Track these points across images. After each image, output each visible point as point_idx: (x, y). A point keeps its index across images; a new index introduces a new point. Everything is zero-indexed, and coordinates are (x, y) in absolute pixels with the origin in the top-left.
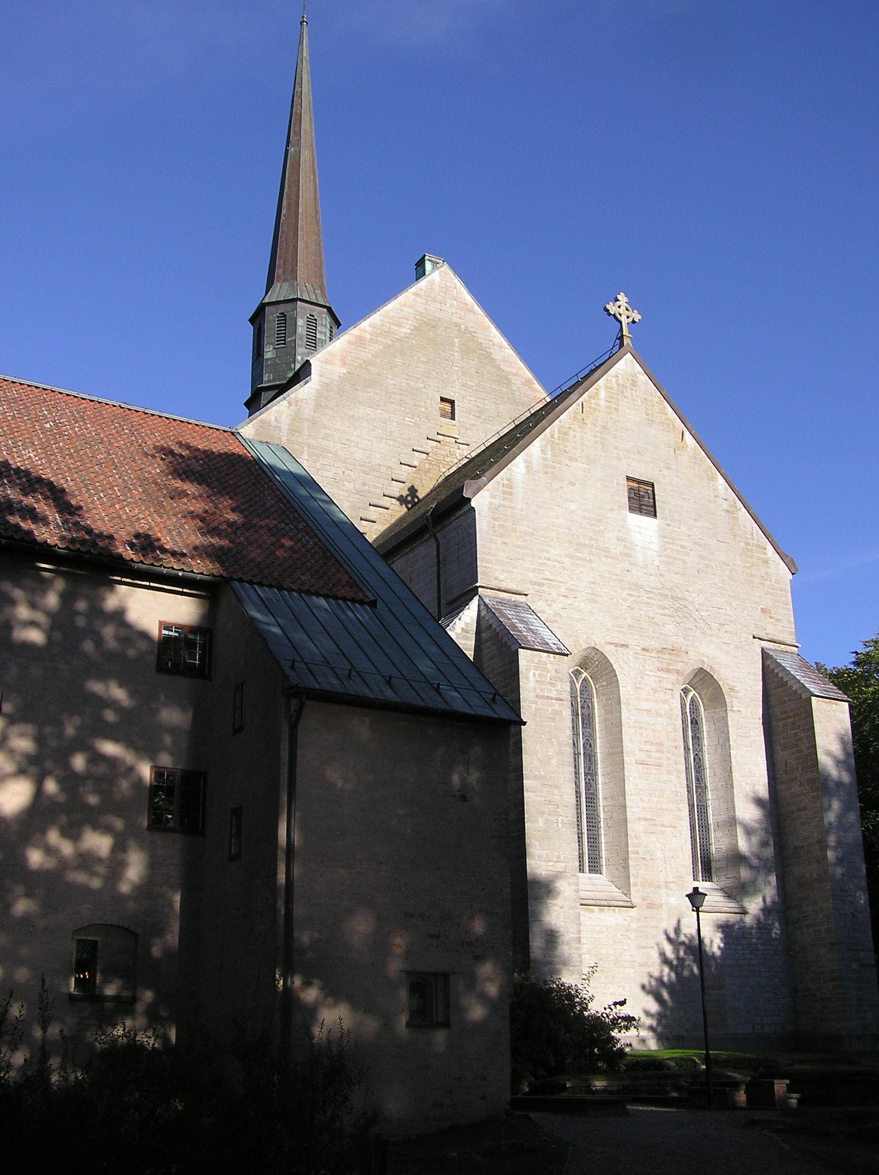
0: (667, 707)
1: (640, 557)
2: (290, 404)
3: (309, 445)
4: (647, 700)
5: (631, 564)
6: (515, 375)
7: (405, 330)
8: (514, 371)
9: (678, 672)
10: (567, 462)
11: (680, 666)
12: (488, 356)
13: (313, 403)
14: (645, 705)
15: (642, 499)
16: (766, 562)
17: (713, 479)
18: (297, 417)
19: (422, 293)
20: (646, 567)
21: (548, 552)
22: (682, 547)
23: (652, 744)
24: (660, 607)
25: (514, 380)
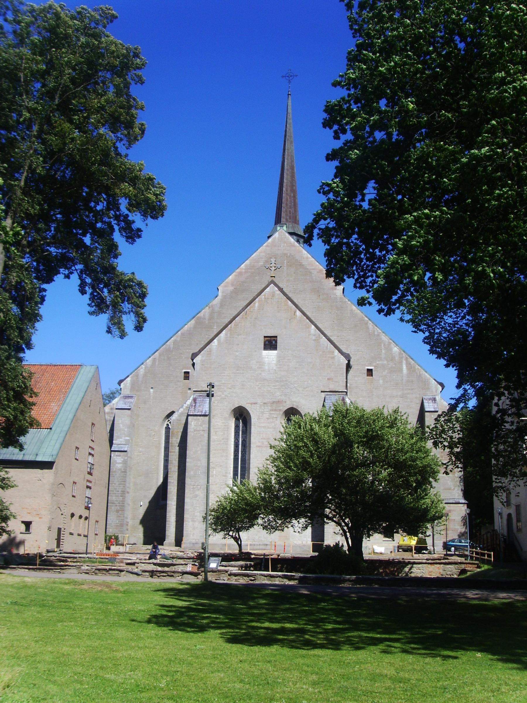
0: (273, 424)
1: (267, 368)
2: (209, 308)
3: (217, 323)
4: (264, 423)
5: (261, 371)
6: (314, 269)
7: (261, 263)
8: (313, 267)
9: (280, 410)
10: (236, 336)
11: (281, 408)
12: (301, 265)
13: (219, 305)
14: (263, 425)
15: (271, 343)
16: (333, 358)
17: (309, 327)
18: (212, 313)
19: (269, 244)
20: (269, 371)
21: (224, 373)
22: (288, 360)
23: (264, 439)
24: (274, 386)
25: (313, 271)
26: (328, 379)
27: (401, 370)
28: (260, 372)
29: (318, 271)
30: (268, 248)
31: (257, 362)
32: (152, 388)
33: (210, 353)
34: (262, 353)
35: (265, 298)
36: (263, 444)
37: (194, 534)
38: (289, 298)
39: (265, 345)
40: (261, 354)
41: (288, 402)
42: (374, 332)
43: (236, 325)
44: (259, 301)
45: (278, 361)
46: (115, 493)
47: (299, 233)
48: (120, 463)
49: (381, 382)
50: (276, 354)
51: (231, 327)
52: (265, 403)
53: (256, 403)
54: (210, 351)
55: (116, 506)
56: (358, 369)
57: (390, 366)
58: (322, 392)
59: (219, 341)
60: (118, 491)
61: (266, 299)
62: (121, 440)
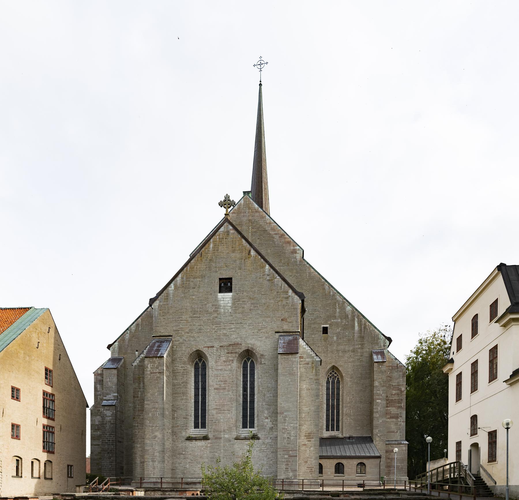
0: (230, 367)
8: (276, 232)
9: (236, 353)
14: (220, 368)
15: (226, 285)
17: (263, 267)
22: (243, 301)
23: (222, 381)
26: (282, 320)
27: (353, 326)
28: (216, 315)
29: (280, 235)
30: (234, 215)
31: (213, 306)
32: (137, 351)
33: (167, 298)
34: (217, 295)
35: (219, 239)
36: (220, 386)
37: (154, 473)
38: (243, 237)
39: (220, 287)
40: (216, 297)
41: (243, 344)
42: (330, 293)
43: (192, 268)
44: (213, 241)
45: (233, 304)
46: (107, 443)
47: (286, 285)
48: (109, 416)
49: (335, 338)
50: (231, 297)
51: (187, 271)
52: (221, 347)
53: (213, 347)
54: (167, 296)
55: (109, 453)
56: (315, 327)
57: (343, 323)
58: (276, 332)
59: (175, 286)
60: (109, 441)
61: (221, 239)
62: (109, 396)
